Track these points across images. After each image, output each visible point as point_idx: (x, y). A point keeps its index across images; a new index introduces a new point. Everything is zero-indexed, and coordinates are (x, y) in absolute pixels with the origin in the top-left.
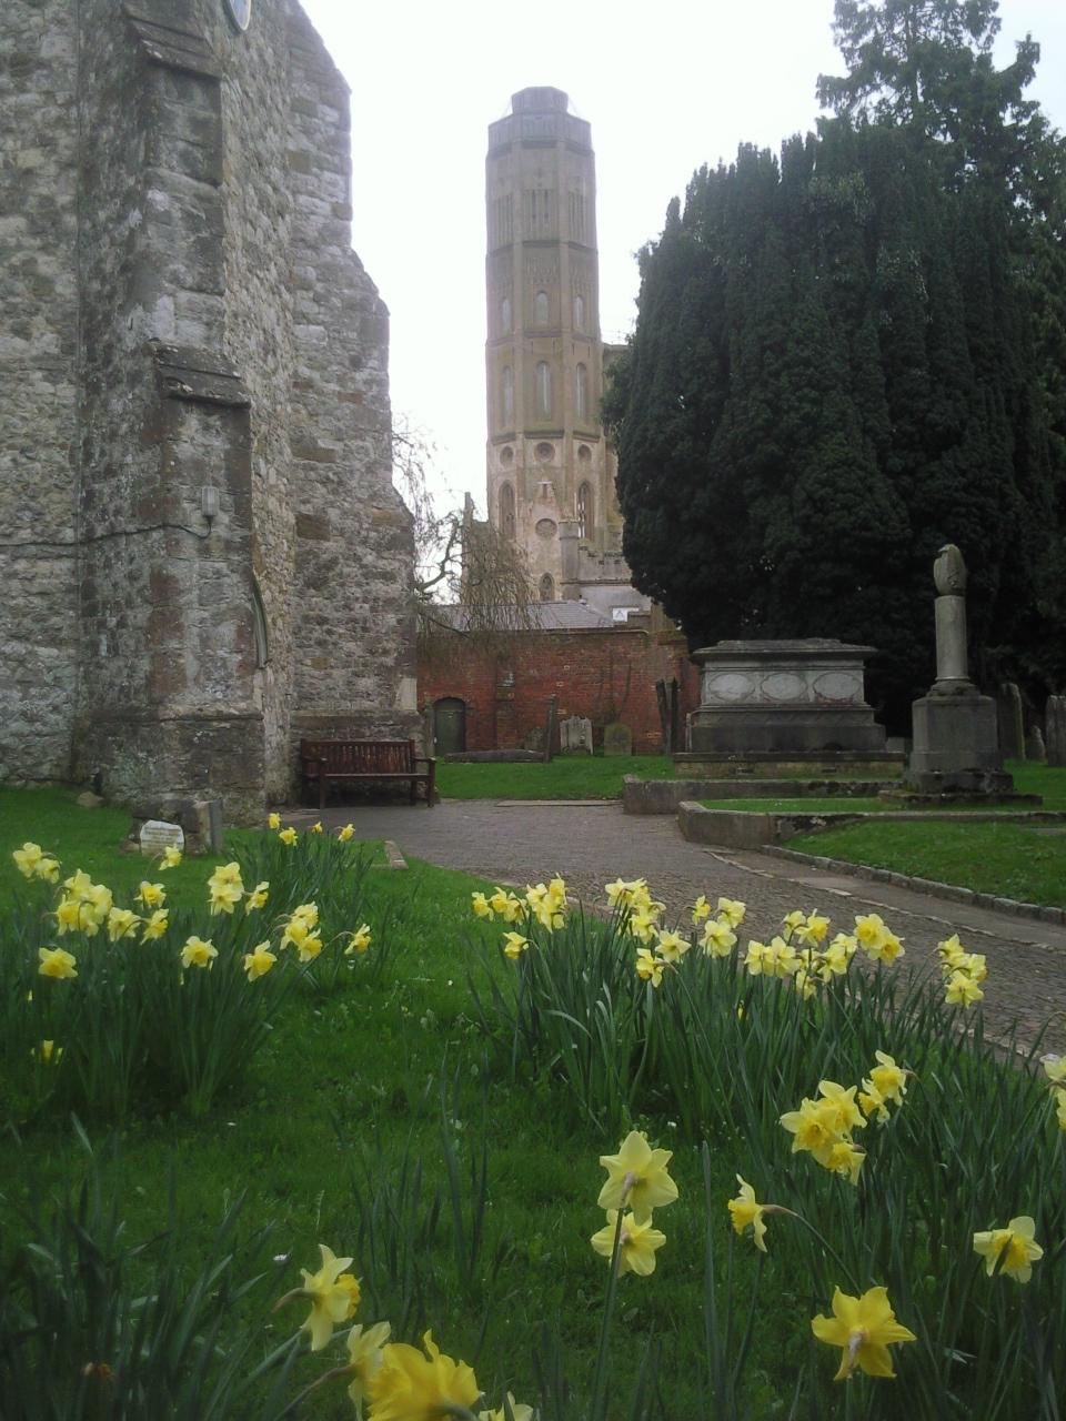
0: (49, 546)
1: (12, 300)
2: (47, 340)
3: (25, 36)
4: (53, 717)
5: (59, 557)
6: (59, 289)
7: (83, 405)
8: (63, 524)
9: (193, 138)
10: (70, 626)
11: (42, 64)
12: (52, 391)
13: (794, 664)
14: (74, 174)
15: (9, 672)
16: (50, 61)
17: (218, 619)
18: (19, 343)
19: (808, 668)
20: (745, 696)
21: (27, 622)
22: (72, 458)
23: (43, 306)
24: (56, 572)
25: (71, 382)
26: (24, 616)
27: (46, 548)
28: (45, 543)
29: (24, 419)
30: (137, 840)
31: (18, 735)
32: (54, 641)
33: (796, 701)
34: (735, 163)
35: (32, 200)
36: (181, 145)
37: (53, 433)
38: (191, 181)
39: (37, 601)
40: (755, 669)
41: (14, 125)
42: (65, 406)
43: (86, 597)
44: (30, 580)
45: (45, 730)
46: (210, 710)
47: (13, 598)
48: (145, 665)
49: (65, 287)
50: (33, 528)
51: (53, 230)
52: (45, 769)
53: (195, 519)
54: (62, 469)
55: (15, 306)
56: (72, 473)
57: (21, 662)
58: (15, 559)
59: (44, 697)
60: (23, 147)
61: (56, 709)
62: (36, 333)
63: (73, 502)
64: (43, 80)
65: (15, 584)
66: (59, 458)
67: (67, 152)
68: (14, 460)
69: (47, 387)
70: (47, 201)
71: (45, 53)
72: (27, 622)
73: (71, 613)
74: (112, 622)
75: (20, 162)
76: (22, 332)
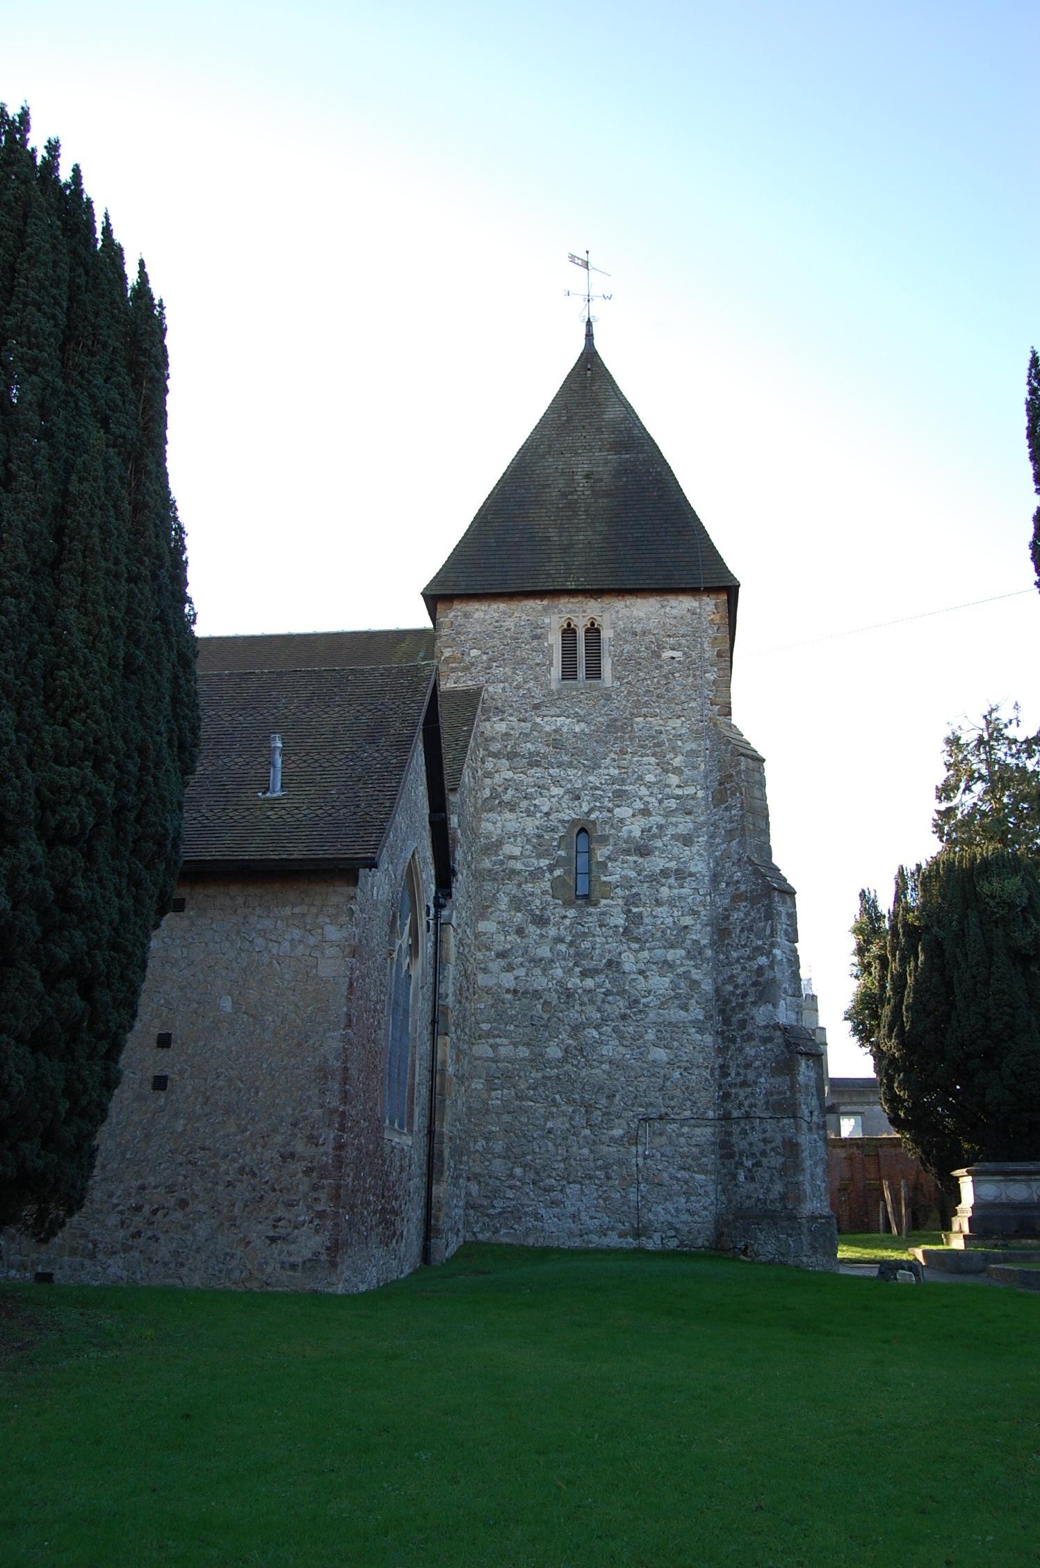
0: (700, 1120)
1: (678, 991)
2: (697, 1013)
3: (682, 860)
4: (704, 1213)
5: (706, 1126)
6: (703, 987)
7: (719, 1047)
8: (708, 1108)
9: (788, 923)
10: (712, 1164)
11: (691, 875)
12: (700, 1038)
13: (1023, 1178)
14: (709, 928)
15: (679, 1188)
16: (695, 873)
17: (816, 1164)
18: (683, 1013)
19: (1031, 1180)
20: (996, 1198)
21: (689, 1160)
22: (712, 1075)
23: (695, 995)
24: (704, 1134)
25: (710, 1034)
26: (687, 1157)
27: (698, 1121)
28: (698, 1118)
29: (686, 1052)
30: (896, 1279)
31: (685, 1223)
32: (705, 1172)
33: (1027, 1201)
34: (924, 866)
35: (689, 942)
36: (784, 926)
37: (701, 1060)
38: (787, 942)
39: (694, 1149)
40: (1002, 1181)
41: (678, 904)
42: (707, 1047)
43: (725, 1149)
44: (690, 1138)
45: (700, 1220)
46: (816, 1214)
47: (682, 1147)
48: (778, 1188)
49: (707, 986)
50: (691, 1110)
51: (699, 957)
52: (700, 1242)
53: (806, 1112)
54: (707, 1080)
55: (680, 994)
56: (712, 1082)
57: (686, 1182)
58: (682, 1126)
59: (699, 1201)
60: (682, 915)
61: (705, 1208)
62: (691, 1009)
63: (713, 1097)
64: (693, 883)
65: (682, 1140)
66: (705, 1074)
67: (705, 918)
68: (681, 1074)
69: (699, 1037)
70: (696, 942)
71: (693, 870)
72: (689, 1160)
73: (713, 1156)
74: (749, 1163)
75: (681, 922)
76: (685, 1008)
